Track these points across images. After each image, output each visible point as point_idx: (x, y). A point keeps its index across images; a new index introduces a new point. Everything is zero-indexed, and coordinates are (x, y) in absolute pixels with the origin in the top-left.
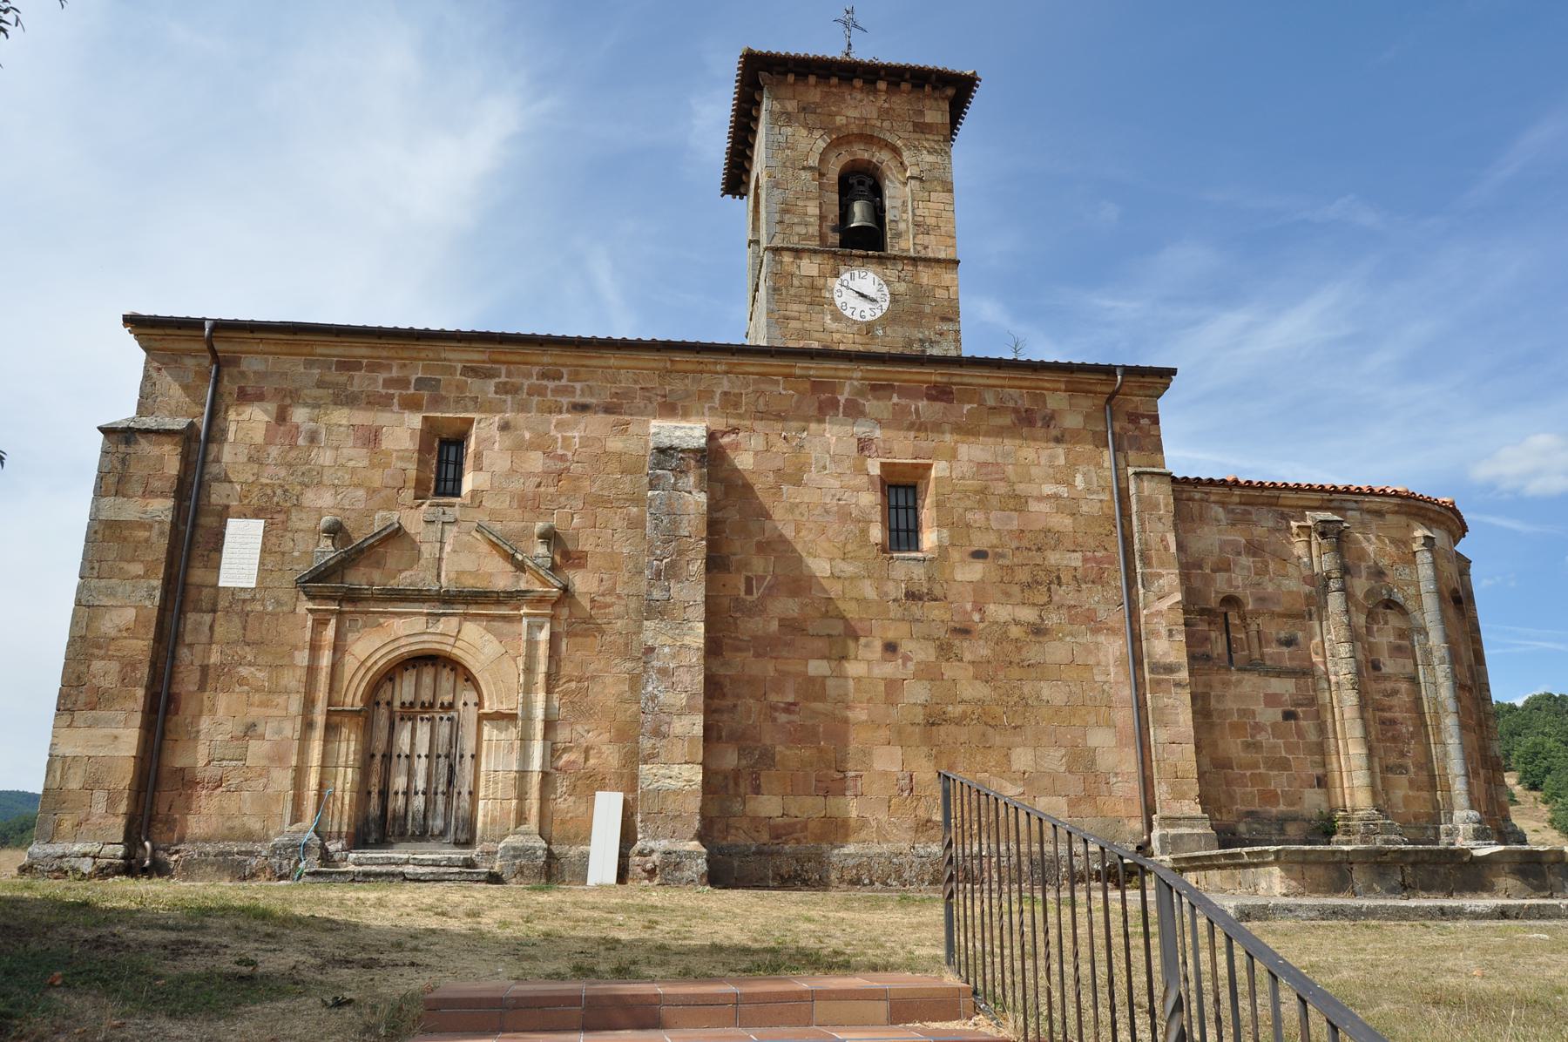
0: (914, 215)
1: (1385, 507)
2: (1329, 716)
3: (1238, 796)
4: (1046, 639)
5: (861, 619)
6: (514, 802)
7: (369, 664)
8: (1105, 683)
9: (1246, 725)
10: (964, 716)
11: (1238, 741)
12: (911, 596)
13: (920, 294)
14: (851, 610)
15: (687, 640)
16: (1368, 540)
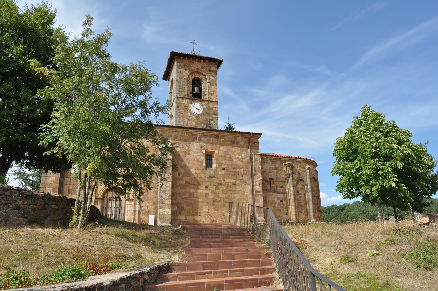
0: (208, 91)
1: (301, 161)
2: (289, 201)
4: (236, 186)
5: (201, 182)
6: (133, 217)
7: (103, 189)
9: (273, 203)
10: (220, 200)
11: (272, 206)
12: (210, 177)
13: (209, 109)
14: (199, 180)
15: (168, 185)
16: (298, 167)
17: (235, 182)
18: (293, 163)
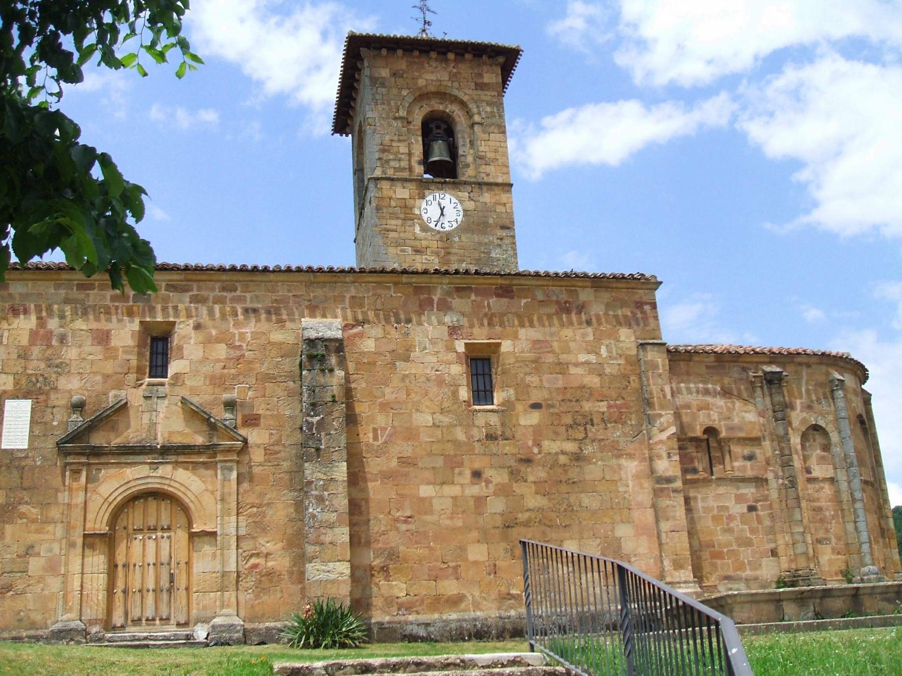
3: (719, 566)
8: (626, 492)
12: (491, 437)
17: (579, 451)
18: (785, 370)
